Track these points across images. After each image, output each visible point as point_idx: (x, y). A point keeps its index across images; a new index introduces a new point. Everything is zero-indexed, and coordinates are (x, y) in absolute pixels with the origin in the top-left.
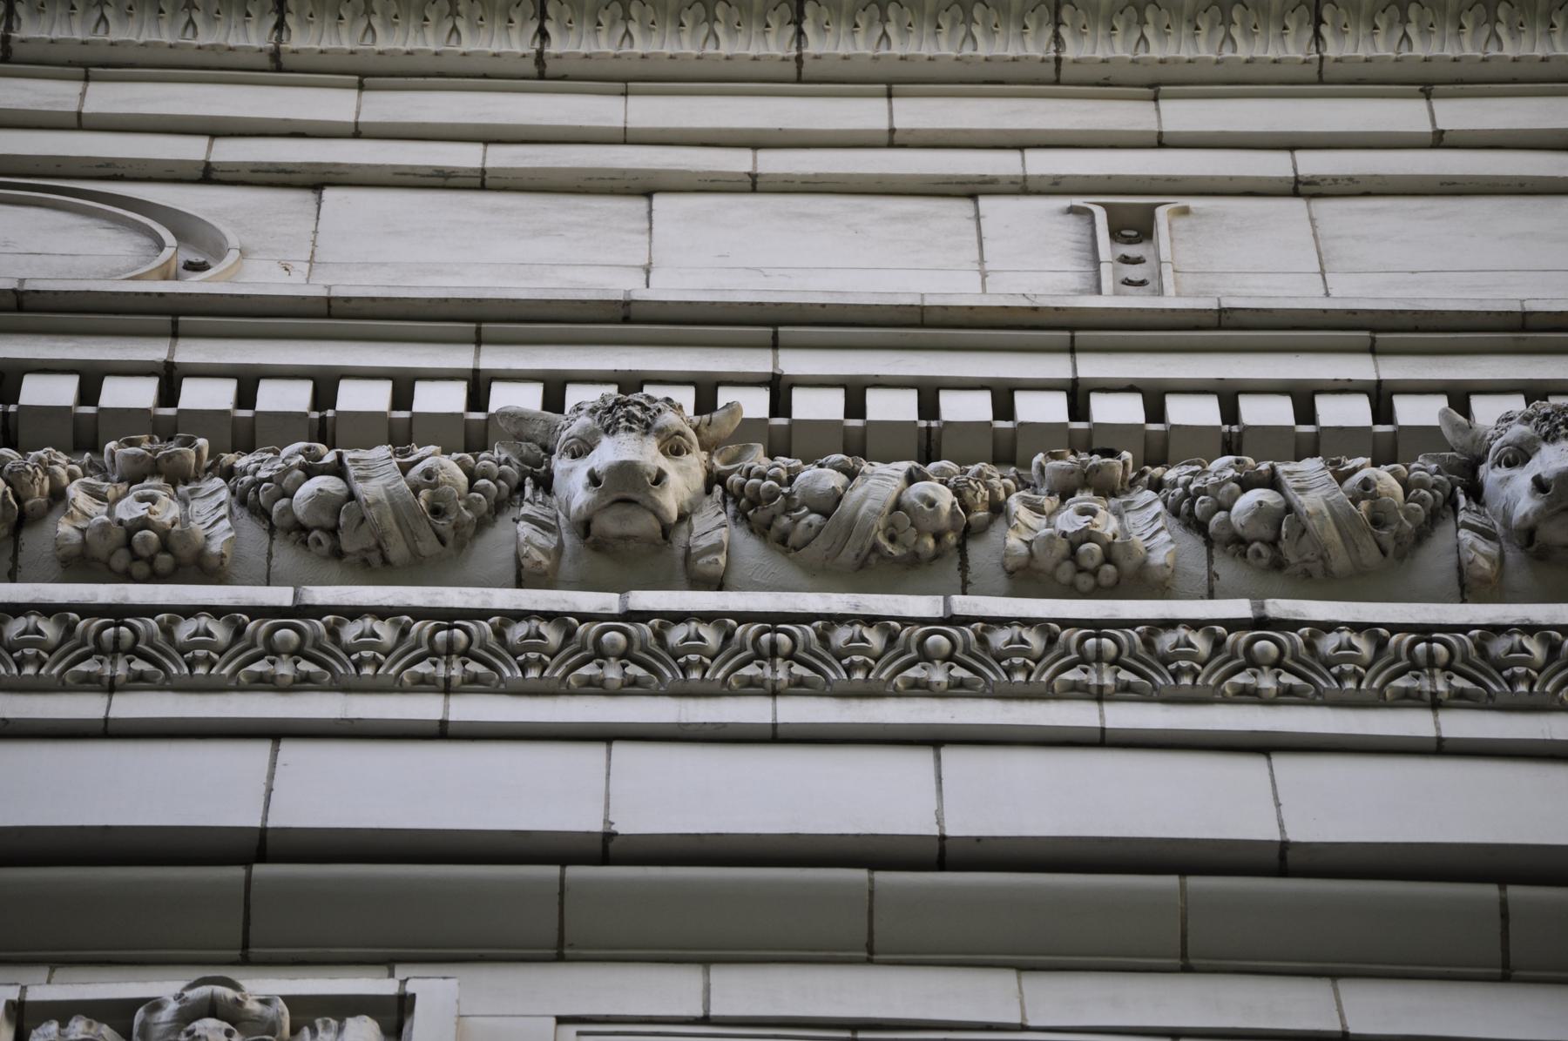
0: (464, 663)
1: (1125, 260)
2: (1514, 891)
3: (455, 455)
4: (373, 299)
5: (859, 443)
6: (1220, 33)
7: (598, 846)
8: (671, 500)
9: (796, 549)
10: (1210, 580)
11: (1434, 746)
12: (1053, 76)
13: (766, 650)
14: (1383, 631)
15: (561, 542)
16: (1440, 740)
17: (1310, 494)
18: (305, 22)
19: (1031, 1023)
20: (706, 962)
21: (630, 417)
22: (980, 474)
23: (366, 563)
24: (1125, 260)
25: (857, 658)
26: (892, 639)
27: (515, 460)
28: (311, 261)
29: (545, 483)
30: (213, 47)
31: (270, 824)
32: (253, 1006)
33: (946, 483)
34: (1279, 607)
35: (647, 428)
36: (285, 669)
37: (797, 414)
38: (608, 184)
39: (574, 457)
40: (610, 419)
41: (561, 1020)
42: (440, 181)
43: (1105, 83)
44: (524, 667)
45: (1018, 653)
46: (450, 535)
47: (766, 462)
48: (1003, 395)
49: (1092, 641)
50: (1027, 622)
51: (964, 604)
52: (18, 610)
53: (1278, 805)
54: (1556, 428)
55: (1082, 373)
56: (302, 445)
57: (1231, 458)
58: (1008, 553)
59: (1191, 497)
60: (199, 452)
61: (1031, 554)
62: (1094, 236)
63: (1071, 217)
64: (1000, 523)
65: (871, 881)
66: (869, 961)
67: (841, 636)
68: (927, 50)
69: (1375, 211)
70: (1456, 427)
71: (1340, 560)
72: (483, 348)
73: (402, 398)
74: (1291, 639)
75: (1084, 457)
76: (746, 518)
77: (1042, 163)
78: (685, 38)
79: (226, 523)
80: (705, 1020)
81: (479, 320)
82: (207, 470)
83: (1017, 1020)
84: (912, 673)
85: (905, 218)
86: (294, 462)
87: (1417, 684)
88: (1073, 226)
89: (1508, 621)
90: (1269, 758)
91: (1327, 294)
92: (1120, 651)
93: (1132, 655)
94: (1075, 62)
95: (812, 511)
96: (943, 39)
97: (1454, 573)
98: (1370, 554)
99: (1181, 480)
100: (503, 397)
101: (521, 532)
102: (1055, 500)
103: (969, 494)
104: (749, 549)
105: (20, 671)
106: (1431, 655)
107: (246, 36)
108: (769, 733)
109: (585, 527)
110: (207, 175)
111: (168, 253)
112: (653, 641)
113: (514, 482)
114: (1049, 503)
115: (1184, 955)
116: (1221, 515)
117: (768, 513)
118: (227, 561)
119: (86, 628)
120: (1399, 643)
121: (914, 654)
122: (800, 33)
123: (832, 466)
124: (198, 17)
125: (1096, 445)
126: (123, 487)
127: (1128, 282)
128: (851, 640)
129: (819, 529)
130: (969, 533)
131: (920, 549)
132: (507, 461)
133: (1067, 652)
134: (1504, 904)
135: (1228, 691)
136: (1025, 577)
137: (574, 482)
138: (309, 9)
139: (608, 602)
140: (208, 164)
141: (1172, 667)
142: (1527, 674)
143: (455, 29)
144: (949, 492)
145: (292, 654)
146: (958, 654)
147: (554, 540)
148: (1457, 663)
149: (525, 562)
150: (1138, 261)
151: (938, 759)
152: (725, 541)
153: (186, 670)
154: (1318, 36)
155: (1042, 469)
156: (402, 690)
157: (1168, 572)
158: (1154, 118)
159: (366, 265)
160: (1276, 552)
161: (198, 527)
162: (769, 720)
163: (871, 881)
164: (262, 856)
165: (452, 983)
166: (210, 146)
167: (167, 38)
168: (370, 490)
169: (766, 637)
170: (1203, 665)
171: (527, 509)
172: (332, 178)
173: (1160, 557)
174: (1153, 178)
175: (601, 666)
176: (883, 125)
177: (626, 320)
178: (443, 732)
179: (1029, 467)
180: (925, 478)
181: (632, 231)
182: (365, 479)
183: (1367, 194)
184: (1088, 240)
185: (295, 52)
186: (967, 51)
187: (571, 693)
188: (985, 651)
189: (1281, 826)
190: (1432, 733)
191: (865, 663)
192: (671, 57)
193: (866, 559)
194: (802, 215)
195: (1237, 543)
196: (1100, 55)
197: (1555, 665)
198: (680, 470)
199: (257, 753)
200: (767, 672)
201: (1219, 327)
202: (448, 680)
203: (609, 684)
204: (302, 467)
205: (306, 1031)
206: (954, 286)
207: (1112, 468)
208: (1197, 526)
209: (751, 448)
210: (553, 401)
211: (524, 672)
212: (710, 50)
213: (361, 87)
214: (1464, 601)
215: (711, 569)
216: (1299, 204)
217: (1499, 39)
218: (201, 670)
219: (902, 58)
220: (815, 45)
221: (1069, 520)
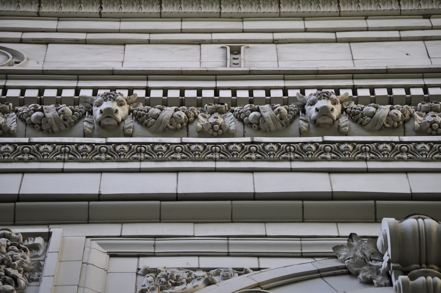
0: (369, 154)
1: (234, 59)
2: (305, 202)
3: (70, 107)
4: (53, 70)
5: (165, 102)
6: (257, 6)
7: (97, 197)
8: (120, 116)
9: (149, 127)
10: (244, 133)
11: (290, 170)
12: (219, 16)
13: (364, 150)
14: (280, 144)
15: (94, 127)
16: (291, 168)
17: (266, 113)
18: (45, 5)
19: (195, 235)
20: (122, 223)
21: (110, 97)
22: (191, 109)
23: (48, 132)
24: (234, 59)
25: (160, 153)
26: (168, 148)
27: (84, 107)
28: (44, 61)
29: (91, 113)
30: (23, 11)
31: (20, 193)
32: (14, 235)
33: (399, 110)
34: (257, 139)
35: (114, 100)
36: (26, 157)
37: (221, 96)
38: (115, 42)
39: (97, 107)
40: (106, 98)
41: (87, 237)
42: (76, 42)
43: (231, 18)
44: (82, 156)
45: (197, 151)
46: (68, 125)
47: (143, 107)
48: (199, 91)
49: (214, 148)
50: (199, 144)
51: (185, 140)
52: (4, 144)
53: (254, 184)
54: (321, 97)
55: (218, 86)
56: (33, 105)
57: (249, 105)
58: (197, 128)
59: (240, 114)
60: (10, 106)
61: (203, 128)
62: (227, 53)
63: (222, 49)
64: (196, 120)
65: (160, 204)
66: (160, 222)
67: (156, 147)
68: (171, 10)
69: (291, 47)
70: (300, 97)
71: (273, 128)
72: (79, 81)
73: (59, 93)
74: (259, 146)
75: (216, 105)
76: (138, 120)
77: (216, 36)
78: (134, 8)
79: (15, 123)
80: (121, 236)
81: (78, 75)
82: (12, 110)
83: (192, 235)
84: (172, 156)
85: (184, 49)
86: (31, 109)
87: (363, 156)
88: (222, 51)
89: (307, 141)
90: (407, 174)
91: (278, 66)
92: (220, 150)
93: (223, 151)
94: (224, 13)
95: (152, 118)
96: (194, 8)
97: (298, 130)
98: (280, 126)
99: (238, 110)
100: (83, 93)
101: (85, 124)
102: (209, 115)
103: (189, 114)
104: (138, 127)
105: (4, 158)
106: (290, 149)
107: (32, 8)
108: (366, 170)
109: (99, 123)
110: (21, 41)
111: (10, 60)
112: (113, 149)
113: (84, 113)
114: (208, 116)
115: (232, 219)
116: (247, 118)
117: (142, 119)
118: (15, 132)
119: (134, 147)
120: (283, 147)
121: (173, 151)
122: (161, 7)
123: (157, 108)
124: (20, 4)
125: (220, 102)
126: (209, 115)
127: (234, 64)
128: (159, 148)
129: (154, 122)
130: (189, 123)
131: (178, 127)
132: (82, 108)
133: (208, 150)
134: (303, 205)
135: (396, 158)
136: (202, 133)
137: (311, 111)
138: (46, 2)
139: (103, 140)
140: (21, 39)
141: (232, 153)
142: (387, 153)
143: (80, 6)
144: (184, 114)
145: (28, 153)
146: (183, 151)
147: (92, 126)
148: (296, 151)
149: (85, 131)
150: (237, 59)
151: (178, 175)
152: (132, 125)
153: (3, 158)
154: (279, 7)
155: (206, 108)
156: (319, 160)
157: (234, 131)
158: (242, 26)
159: (57, 62)
160: (259, 126)
161: (8, 124)
162: (139, 167)
163: (160, 204)
164: (18, 201)
165: (61, 229)
166: (22, 35)
167: (13, 9)
168: (49, 115)
169: (139, 148)
170: (239, 153)
171: (86, 119)
172: (50, 42)
173: (232, 128)
174: (241, 40)
175: (100, 155)
176: (180, 28)
177: (113, 74)
178: (63, 171)
179: (417, 106)
180: (179, 110)
181: (120, 53)
182: (48, 112)
183: (289, 43)
184: (225, 54)
185: (43, 12)
186: (200, 11)
187: (93, 162)
188: (190, 150)
189: (254, 189)
190: (289, 167)
191: (162, 154)
192: (131, 13)
193: (165, 129)
194: (160, 49)
195: (250, 124)
196: (230, 11)
197: (243, 151)
198: (122, 109)
199: (18, 177)
200: (139, 156)
201: (249, 74)
202: (64, 159)
203: (102, 160)
204: (33, 110)
205: (26, 240)
206: (192, 65)
207: (222, 107)
208: (241, 120)
209: (139, 104)
210: (303, 93)
211: (82, 157)
212: (140, 11)
213: (58, 20)
214: (300, 137)
215: (129, 132)
216: (274, 45)
217: (320, 7)
218: (6, 158)
219: (184, 12)
220: (105, 10)
221: (212, 120)
